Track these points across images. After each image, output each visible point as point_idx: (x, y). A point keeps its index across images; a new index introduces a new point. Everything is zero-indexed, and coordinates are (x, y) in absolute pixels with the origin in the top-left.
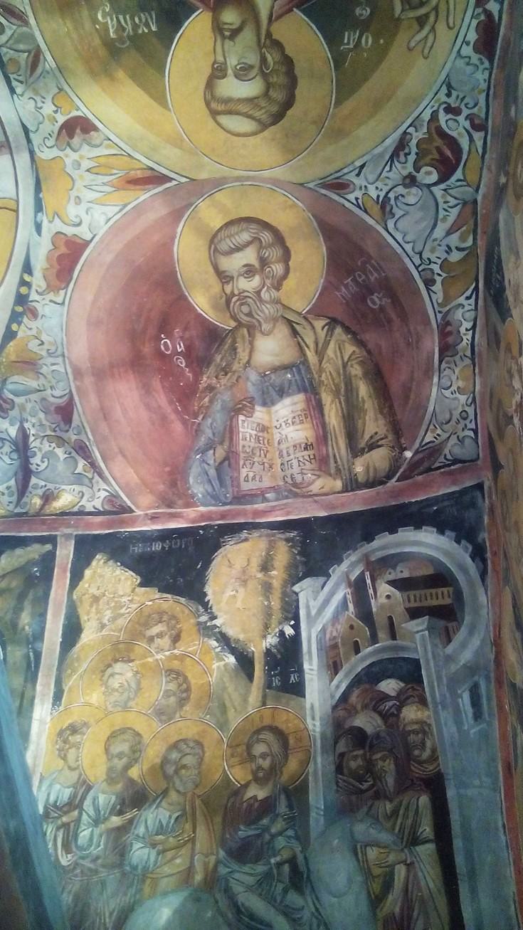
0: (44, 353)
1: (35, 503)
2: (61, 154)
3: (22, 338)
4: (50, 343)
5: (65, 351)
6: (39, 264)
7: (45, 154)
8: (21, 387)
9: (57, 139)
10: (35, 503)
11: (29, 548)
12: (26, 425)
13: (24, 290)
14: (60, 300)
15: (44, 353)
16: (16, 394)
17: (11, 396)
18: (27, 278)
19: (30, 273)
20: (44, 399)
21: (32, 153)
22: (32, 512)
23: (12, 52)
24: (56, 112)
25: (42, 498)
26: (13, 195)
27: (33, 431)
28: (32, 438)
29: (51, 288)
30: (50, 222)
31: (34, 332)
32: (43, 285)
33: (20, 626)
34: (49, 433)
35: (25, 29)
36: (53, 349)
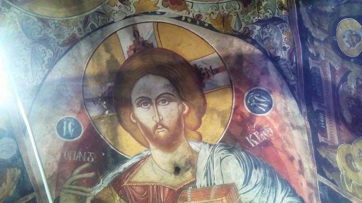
0: (217, 12)
1: (284, 13)
2: (132, 3)
3: (211, 22)
4: (212, 9)
5: (215, 2)
6: (176, 13)
7: (134, 10)
8: (237, 24)
9: (127, 5)
10: (284, 13)
11: (302, 13)
12: (254, 21)
13: (189, 20)
14: (191, 4)
15: (217, 12)
16: (241, 26)
17: (242, 28)
18: (184, 19)
19: (181, 17)
20: (242, 13)
21: (134, 16)
22: (288, 14)
23: (100, 22)
24: (117, 6)
25: (282, 10)
26: (152, 23)
27: (257, 18)
28: (260, 18)
29: (186, 8)
30: (159, 8)
31: (208, 16)
32: (185, 11)
33: (332, 11)
34: (256, 10)
35: (90, 16)
36: (215, 8)
